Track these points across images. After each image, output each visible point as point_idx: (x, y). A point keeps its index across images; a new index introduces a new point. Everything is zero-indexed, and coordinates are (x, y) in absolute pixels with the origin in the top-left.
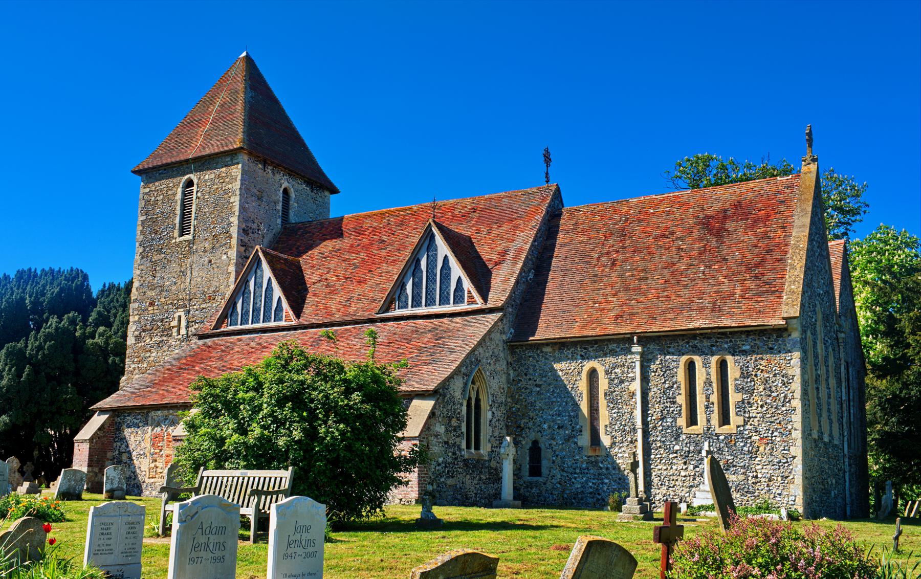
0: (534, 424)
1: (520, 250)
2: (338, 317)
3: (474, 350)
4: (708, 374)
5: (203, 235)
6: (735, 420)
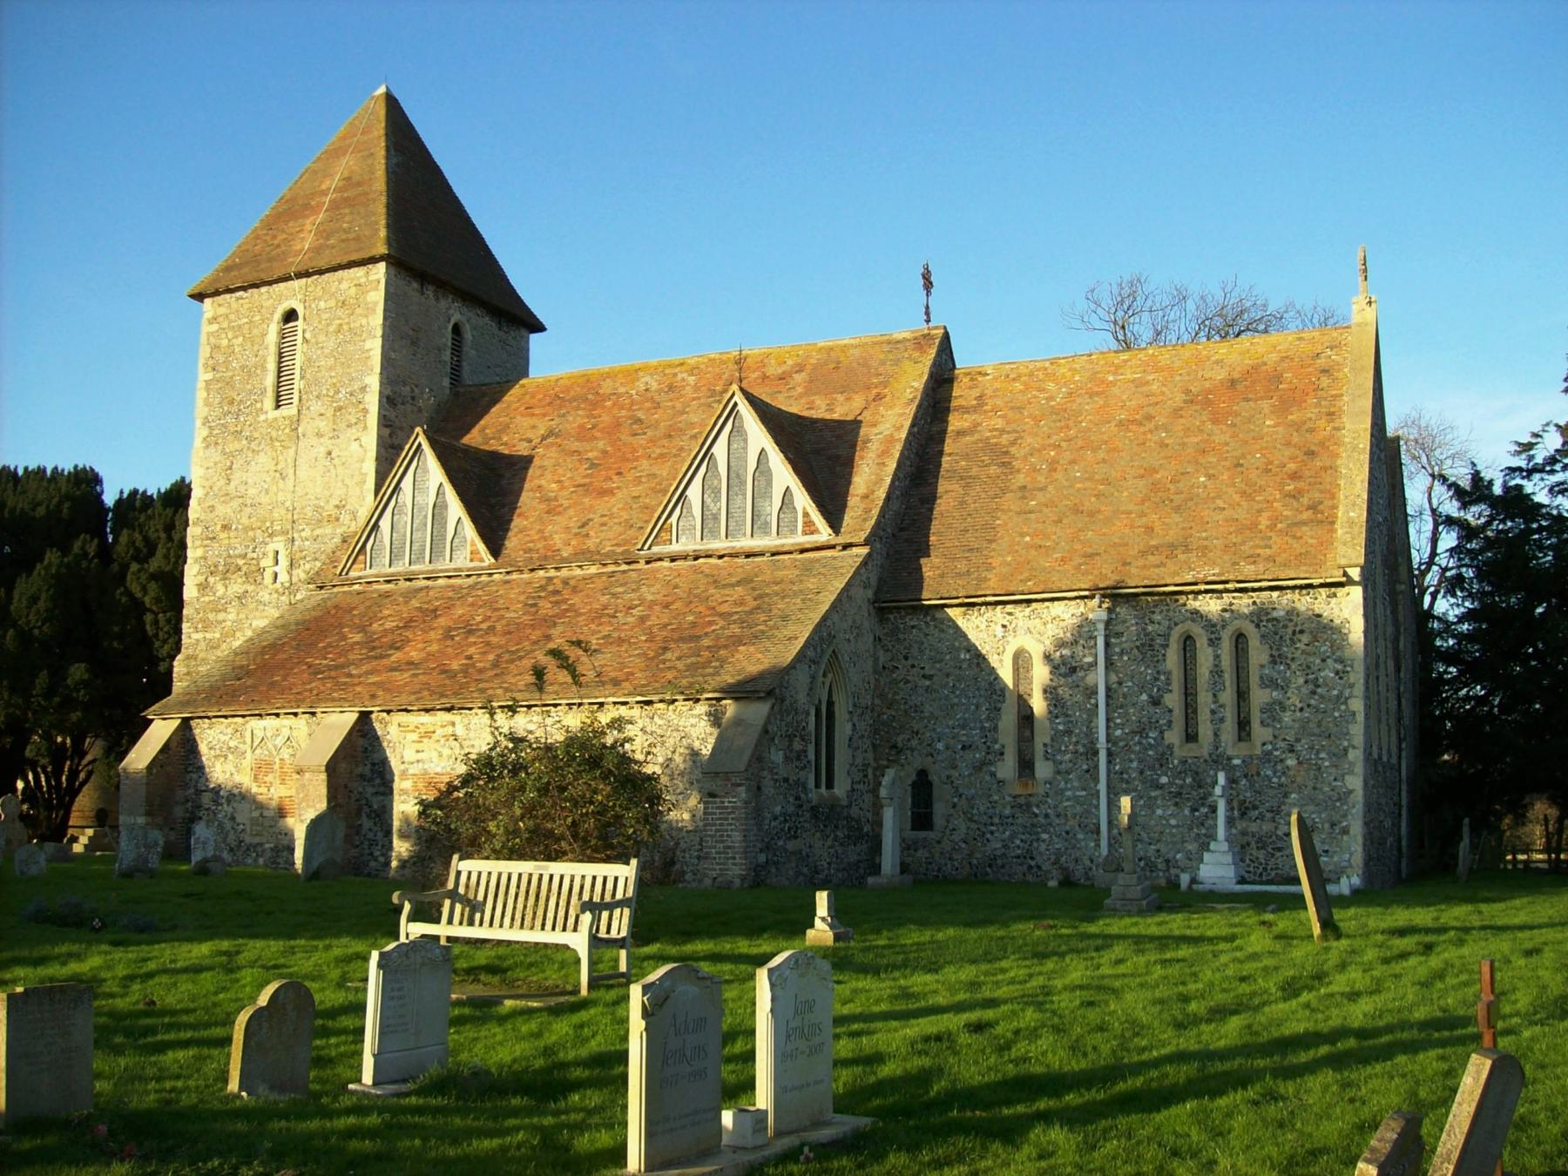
0: (921, 742)
1: (890, 440)
3: (824, 618)
4: (1217, 657)
5: (316, 407)
6: (1260, 733)
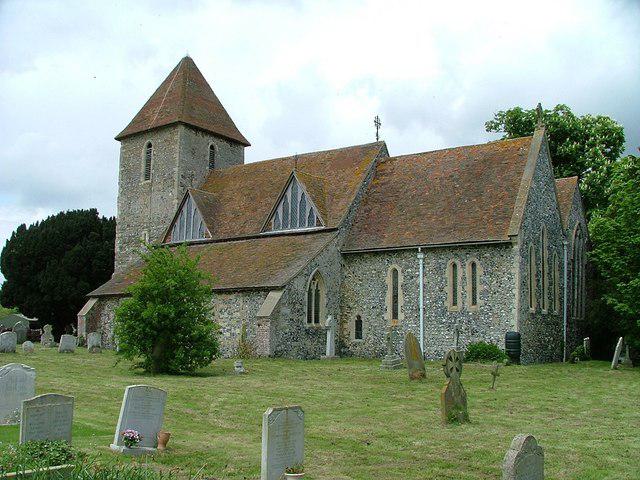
2: (237, 235)
